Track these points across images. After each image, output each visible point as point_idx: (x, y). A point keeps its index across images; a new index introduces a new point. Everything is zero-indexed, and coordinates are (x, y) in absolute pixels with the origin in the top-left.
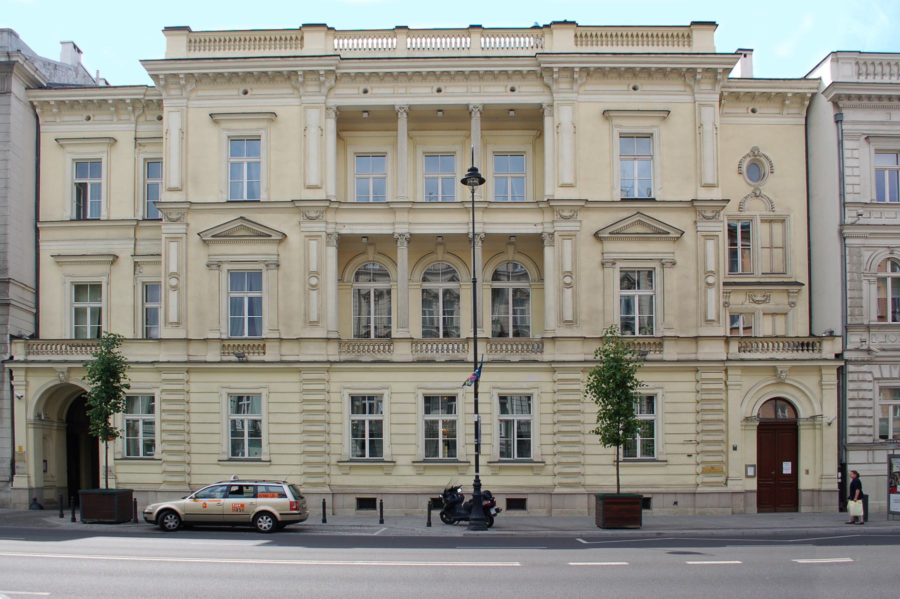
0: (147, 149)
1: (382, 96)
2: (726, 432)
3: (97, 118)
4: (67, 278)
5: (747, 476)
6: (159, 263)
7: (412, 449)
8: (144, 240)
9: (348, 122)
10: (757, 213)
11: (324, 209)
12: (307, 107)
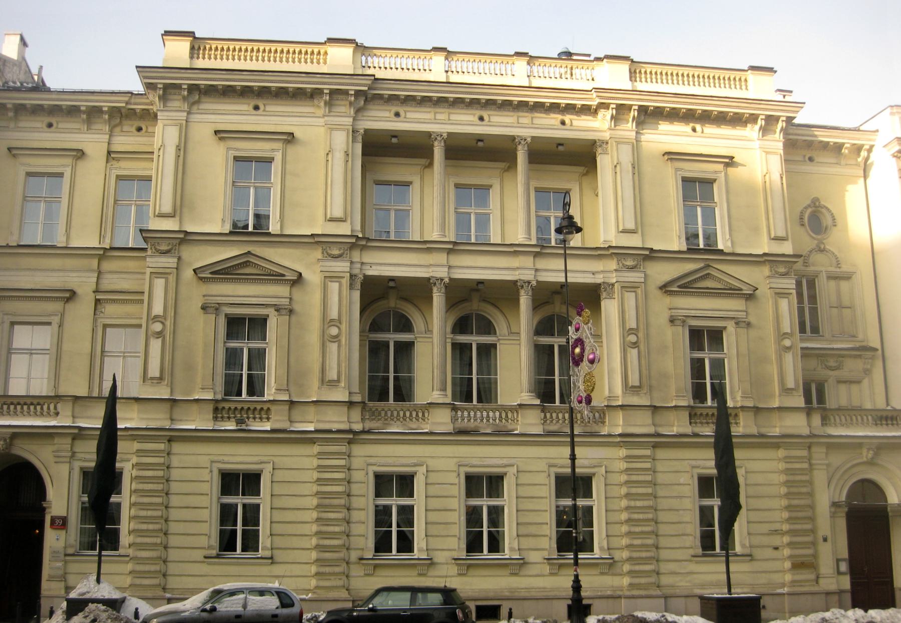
0: (123, 164)
1: (416, 121)
2: (812, 519)
3: (61, 125)
4: (6, 317)
5: (839, 573)
6: (142, 301)
7: (203, 541)
8: (110, 272)
9: (377, 149)
10: (823, 269)
11: (177, 241)
12: (332, 129)
